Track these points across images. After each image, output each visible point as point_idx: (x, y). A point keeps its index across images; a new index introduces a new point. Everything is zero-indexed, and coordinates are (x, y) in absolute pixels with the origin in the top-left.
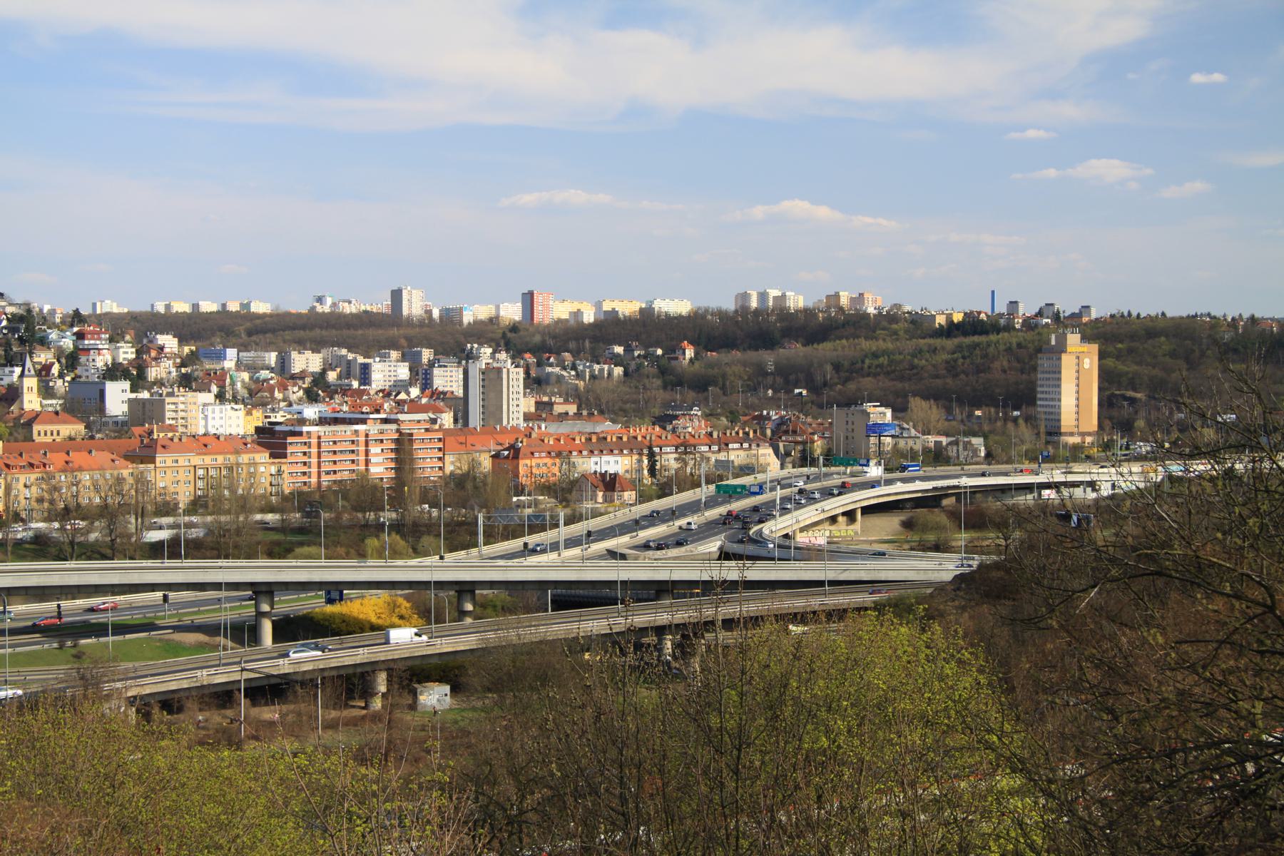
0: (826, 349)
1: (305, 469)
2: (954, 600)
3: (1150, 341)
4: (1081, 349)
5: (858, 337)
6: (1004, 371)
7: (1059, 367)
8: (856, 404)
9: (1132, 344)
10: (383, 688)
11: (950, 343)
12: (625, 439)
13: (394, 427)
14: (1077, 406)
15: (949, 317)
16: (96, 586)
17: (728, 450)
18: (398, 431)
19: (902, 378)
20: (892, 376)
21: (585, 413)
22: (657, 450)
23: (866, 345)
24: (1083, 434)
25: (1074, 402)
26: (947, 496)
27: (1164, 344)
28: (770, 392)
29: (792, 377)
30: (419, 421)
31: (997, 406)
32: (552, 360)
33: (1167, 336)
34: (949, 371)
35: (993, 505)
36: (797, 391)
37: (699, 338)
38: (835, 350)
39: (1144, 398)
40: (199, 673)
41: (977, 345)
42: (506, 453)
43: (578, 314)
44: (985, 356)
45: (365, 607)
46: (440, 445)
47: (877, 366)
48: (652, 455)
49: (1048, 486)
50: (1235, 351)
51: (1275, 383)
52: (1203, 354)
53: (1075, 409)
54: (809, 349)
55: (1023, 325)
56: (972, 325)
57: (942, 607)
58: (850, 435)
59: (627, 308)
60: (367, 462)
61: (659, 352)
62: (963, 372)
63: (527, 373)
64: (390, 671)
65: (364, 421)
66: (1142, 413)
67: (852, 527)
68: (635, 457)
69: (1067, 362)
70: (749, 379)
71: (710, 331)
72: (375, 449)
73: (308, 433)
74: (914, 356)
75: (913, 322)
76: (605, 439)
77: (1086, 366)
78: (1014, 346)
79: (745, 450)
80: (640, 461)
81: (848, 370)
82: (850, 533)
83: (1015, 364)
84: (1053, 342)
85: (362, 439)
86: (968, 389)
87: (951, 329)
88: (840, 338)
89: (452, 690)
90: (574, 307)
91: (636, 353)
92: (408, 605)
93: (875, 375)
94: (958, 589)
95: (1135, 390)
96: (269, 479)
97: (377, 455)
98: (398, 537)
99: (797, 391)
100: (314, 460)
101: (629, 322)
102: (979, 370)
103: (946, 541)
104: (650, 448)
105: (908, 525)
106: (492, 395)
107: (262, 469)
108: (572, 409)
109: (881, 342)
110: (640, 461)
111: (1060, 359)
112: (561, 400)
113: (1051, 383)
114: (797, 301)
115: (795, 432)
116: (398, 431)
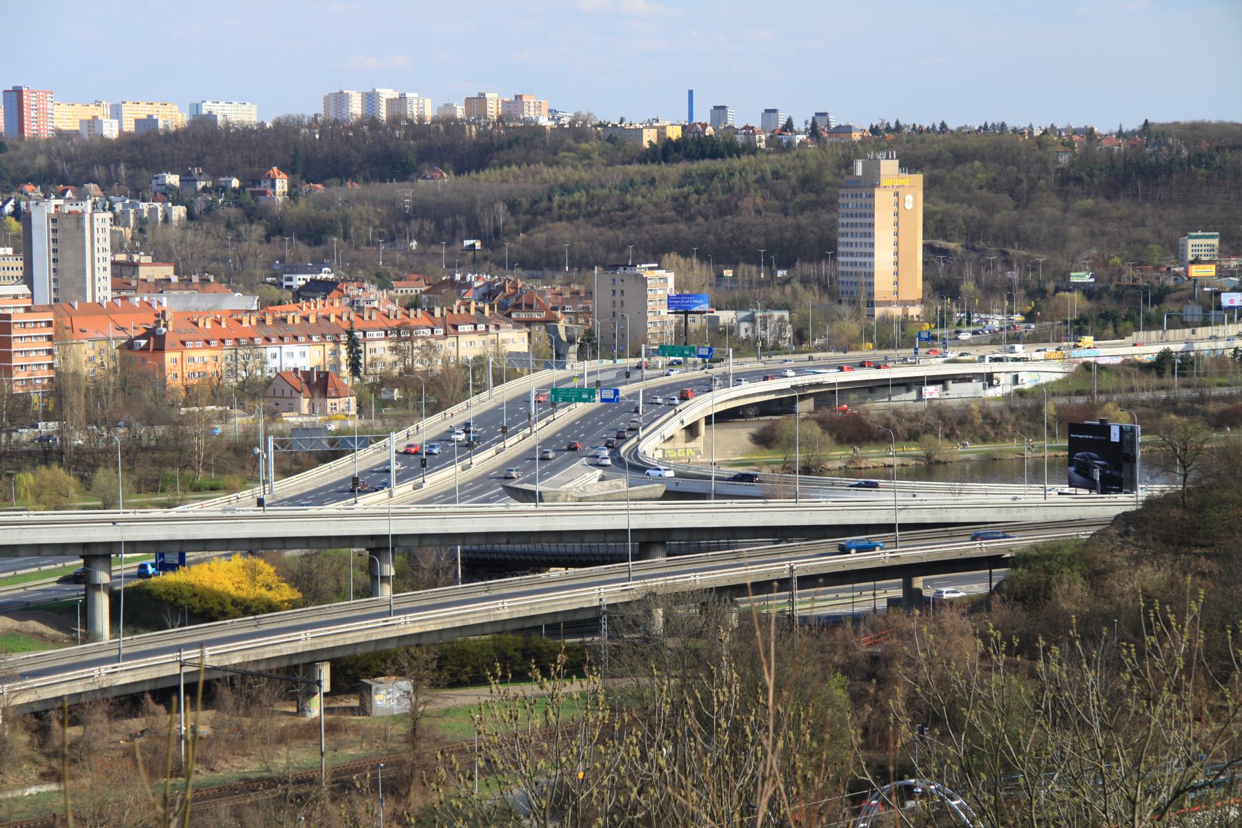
0: (489, 182)
2: (1122, 549)
3: (959, 168)
4: (901, 182)
5: (536, 162)
6: (758, 212)
7: (872, 206)
8: (626, 266)
9: (936, 172)
10: (326, 686)
11: (674, 170)
12: (312, 320)
14: (896, 263)
15: (661, 131)
19: (611, 223)
20: (596, 219)
21: (195, 279)
22: (359, 335)
23: (548, 173)
24: (905, 304)
25: (892, 258)
26: (802, 398)
27: (980, 172)
28: (414, 244)
29: (448, 222)
30: (16, 297)
31: (759, 265)
33: (983, 159)
34: (680, 213)
35: (877, 406)
36: (467, 243)
37: (294, 163)
38: (504, 181)
39: (960, 249)
40: (95, 670)
41: (712, 175)
42: (143, 342)
43: (93, 123)
44: (730, 190)
45: (219, 575)
46: (50, 332)
47: (572, 205)
48: (353, 344)
49: (934, 380)
50: (1078, 180)
51: (1135, 225)
52: (1033, 187)
53: (892, 268)
54: (464, 180)
55: (768, 143)
56: (692, 146)
57: (1108, 558)
58: (618, 309)
59: (172, 117)
61: (235, 183)
62: (699, 213)
66: (969, 272)
67: (692, 444)
68: (330, 346)
69: (883, 200)
70: (382, 225)
71: (282, 146)
74: (624, 190)
75: (611, 139)
76: (285, 320)
77: (909, 206)
78: (769, 176)
79: (481, 334)
80: (335, 353)
81: (532, 211)
82: (690, 452)
83: (774, 202)
84: (859, 172)
86: (711, 237)
87: (667, 151)
88: (509, 164)
90: (88, 113)
91: (200, 185)
92: (272, 570)
93: (571, 219)
94: (1127, 533)
95: (946, 238)
98: (62, 471)
99: (467, 243)
101: (173, 137)
102: (724, 211)
103: (819, 462)
104: (350, 333)
105: (763, 440)
106: (68, 254)
108: (167, 271)
109: (569, 169)
110: (335, 353)
111: (872, 196)
112: (149, 259)
113: (859, 230)
114: (424, 107)
115: (530, 307)
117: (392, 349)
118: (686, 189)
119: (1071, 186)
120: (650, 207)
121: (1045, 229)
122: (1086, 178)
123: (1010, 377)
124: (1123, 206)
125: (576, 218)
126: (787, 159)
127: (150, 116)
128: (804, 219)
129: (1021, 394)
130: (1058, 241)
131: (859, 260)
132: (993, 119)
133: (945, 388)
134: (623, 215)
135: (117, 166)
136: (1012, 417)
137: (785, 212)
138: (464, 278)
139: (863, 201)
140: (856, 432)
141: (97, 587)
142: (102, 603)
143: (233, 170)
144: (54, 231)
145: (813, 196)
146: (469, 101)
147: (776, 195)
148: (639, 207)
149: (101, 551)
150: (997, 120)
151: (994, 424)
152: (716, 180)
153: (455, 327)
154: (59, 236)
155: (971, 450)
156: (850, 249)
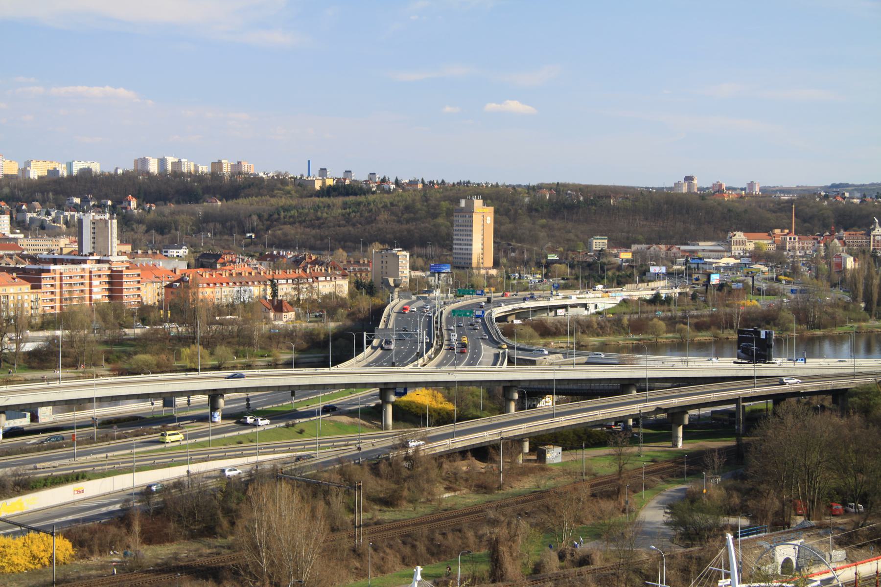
0: (243, 204)
1: (52, 297)
7: (472, 222)
11: (339, 200)
12: (253, 274)
13: (107, 266)
16: (279, 387)
17: (318, 282)
18: (110, 268)
19: (312, 226)
21: (150, 252)
23: (273, 201)
25: (481, 246)
32: (24, 207)
36: (248, 235)
41: (359, 204)
44: (371, 211)
47: (290, 217)
50: (536, 210)
56: (341, 190)
58: (384, 270)
60: (91, 292)
63: (11, 218)
64: (529, 438)
65: (85, 262)
68: (262, 287)
69: (477, 219)
72: (96, 282)
73: (54, 270)
76: (241, 274)
77: (488, 222)
80: (265, 290)
81: (271, 219)
85: (87, 274)
87: (327, 191)
89: (563, 450)
91: (92, 203)
93: (291, 224)
96: (31, 304)
97: (97, 286)
99: (248, 235)
100: (58, 290)
106: (100, 240)
107: (26, 297)
113: (465, 233)
116: (110, 268)
117: (295, 289)
118: (348, 210)
119: (534, 213)
120: (331, 219)
121: (528, 233)
122: (540, 209)
123: (594, 305)
124: (557, 223)
125: (294, 223)
126: (387, 199)
127: (55, 168)
128: (411, 226)
129: (599, 313)
130: (535, 240)
131: (464, 247)
132: (464, 179)
133: (567, 310)
134: (317, 223)
135: (48, 193)
136: (608, 325)
137: (399, 222)
138: (279, 253)
139: (467, 219)
140: (545, 331)
141: (389, 402)
142: (390, 409)
143: (507, 213)
144: (94, 228)
145: (412, 215)
146: (213, 164)
147: (393, 213)
148: (326, 218)
149: (392, 386)
150: (466, 180)
151: (602, 328)
152: (362, 206)
153: (317, 278)
154: (96, 231)
155: (594, 340)
156: (459, 242)
